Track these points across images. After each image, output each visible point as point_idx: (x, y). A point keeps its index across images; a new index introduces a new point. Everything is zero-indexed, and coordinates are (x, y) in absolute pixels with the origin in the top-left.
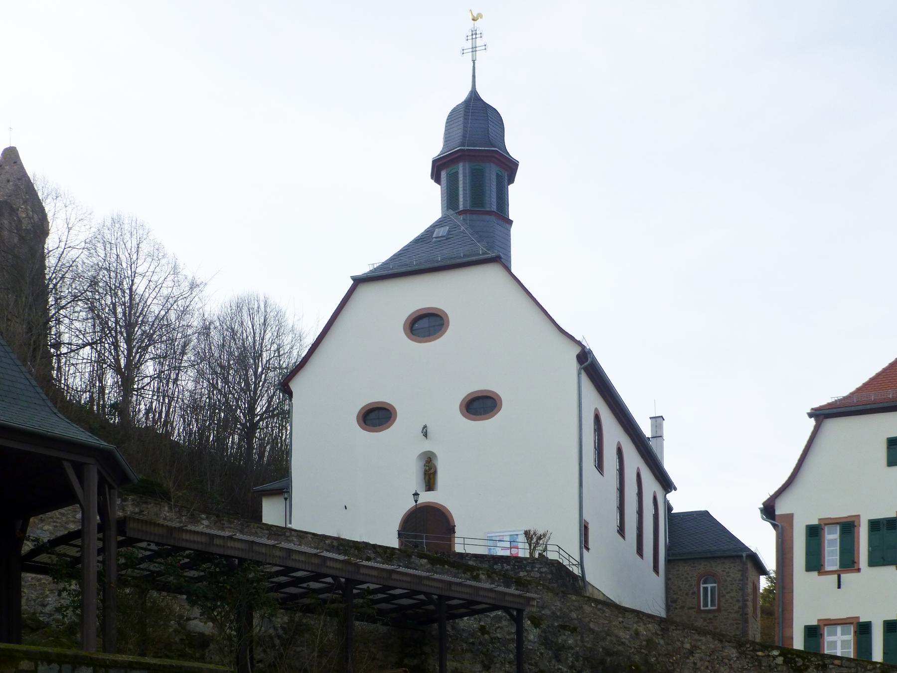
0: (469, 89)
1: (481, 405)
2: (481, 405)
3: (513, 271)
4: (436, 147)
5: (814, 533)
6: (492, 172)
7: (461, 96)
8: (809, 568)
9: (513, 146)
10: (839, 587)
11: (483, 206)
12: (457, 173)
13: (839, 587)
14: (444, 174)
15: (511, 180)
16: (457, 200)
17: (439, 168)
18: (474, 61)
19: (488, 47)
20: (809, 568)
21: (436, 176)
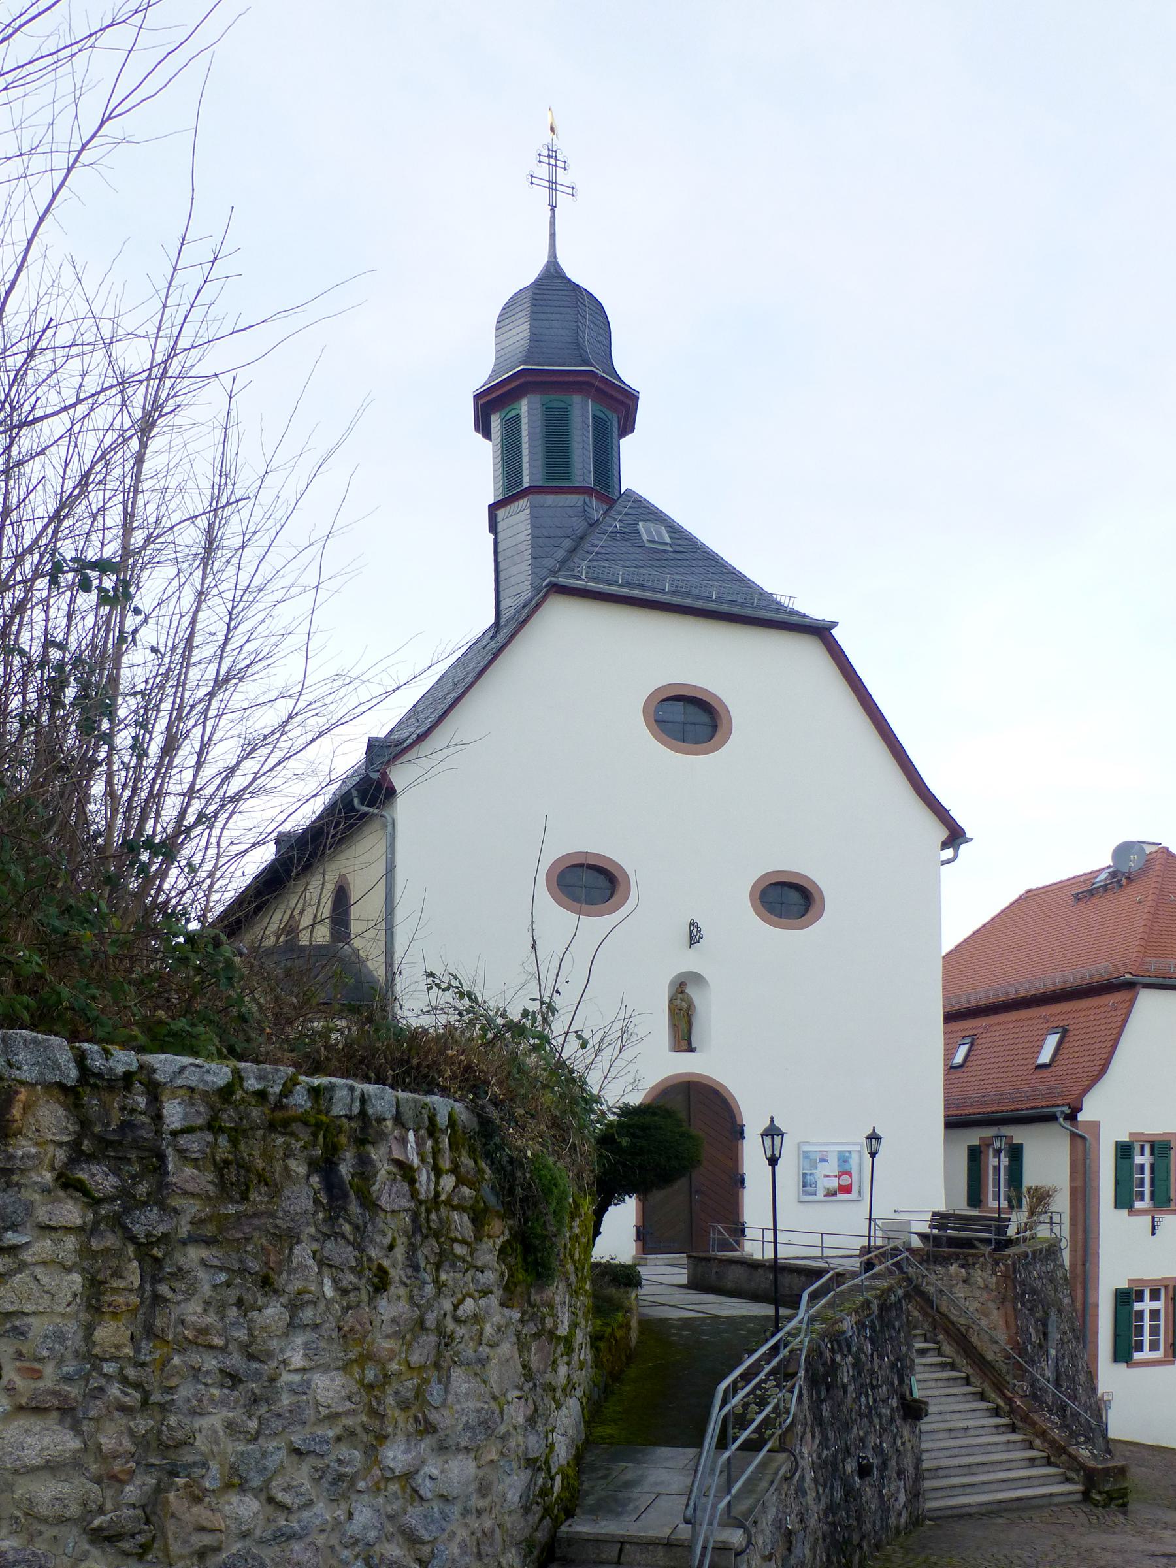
0: (544, 259)
1: (788, 899)
2: (788, 899)
3: (607, 1217)
4: (480, 369)
5: (1124, 1151)
6: (582, 412)
7: (530, 273)
8: (1118, 1205)
9: (629, 364)
10: (1153, 1234)
11: (567, 476)
12: (518, 417)
13: (1153, 1234)
14: (496, 422)
15: (627, 426)
16: (520, 454)
17: (491, 405)
18: (553, 208)
19: (579, 192)
20: (1118, 1205)
21: (483, 427)
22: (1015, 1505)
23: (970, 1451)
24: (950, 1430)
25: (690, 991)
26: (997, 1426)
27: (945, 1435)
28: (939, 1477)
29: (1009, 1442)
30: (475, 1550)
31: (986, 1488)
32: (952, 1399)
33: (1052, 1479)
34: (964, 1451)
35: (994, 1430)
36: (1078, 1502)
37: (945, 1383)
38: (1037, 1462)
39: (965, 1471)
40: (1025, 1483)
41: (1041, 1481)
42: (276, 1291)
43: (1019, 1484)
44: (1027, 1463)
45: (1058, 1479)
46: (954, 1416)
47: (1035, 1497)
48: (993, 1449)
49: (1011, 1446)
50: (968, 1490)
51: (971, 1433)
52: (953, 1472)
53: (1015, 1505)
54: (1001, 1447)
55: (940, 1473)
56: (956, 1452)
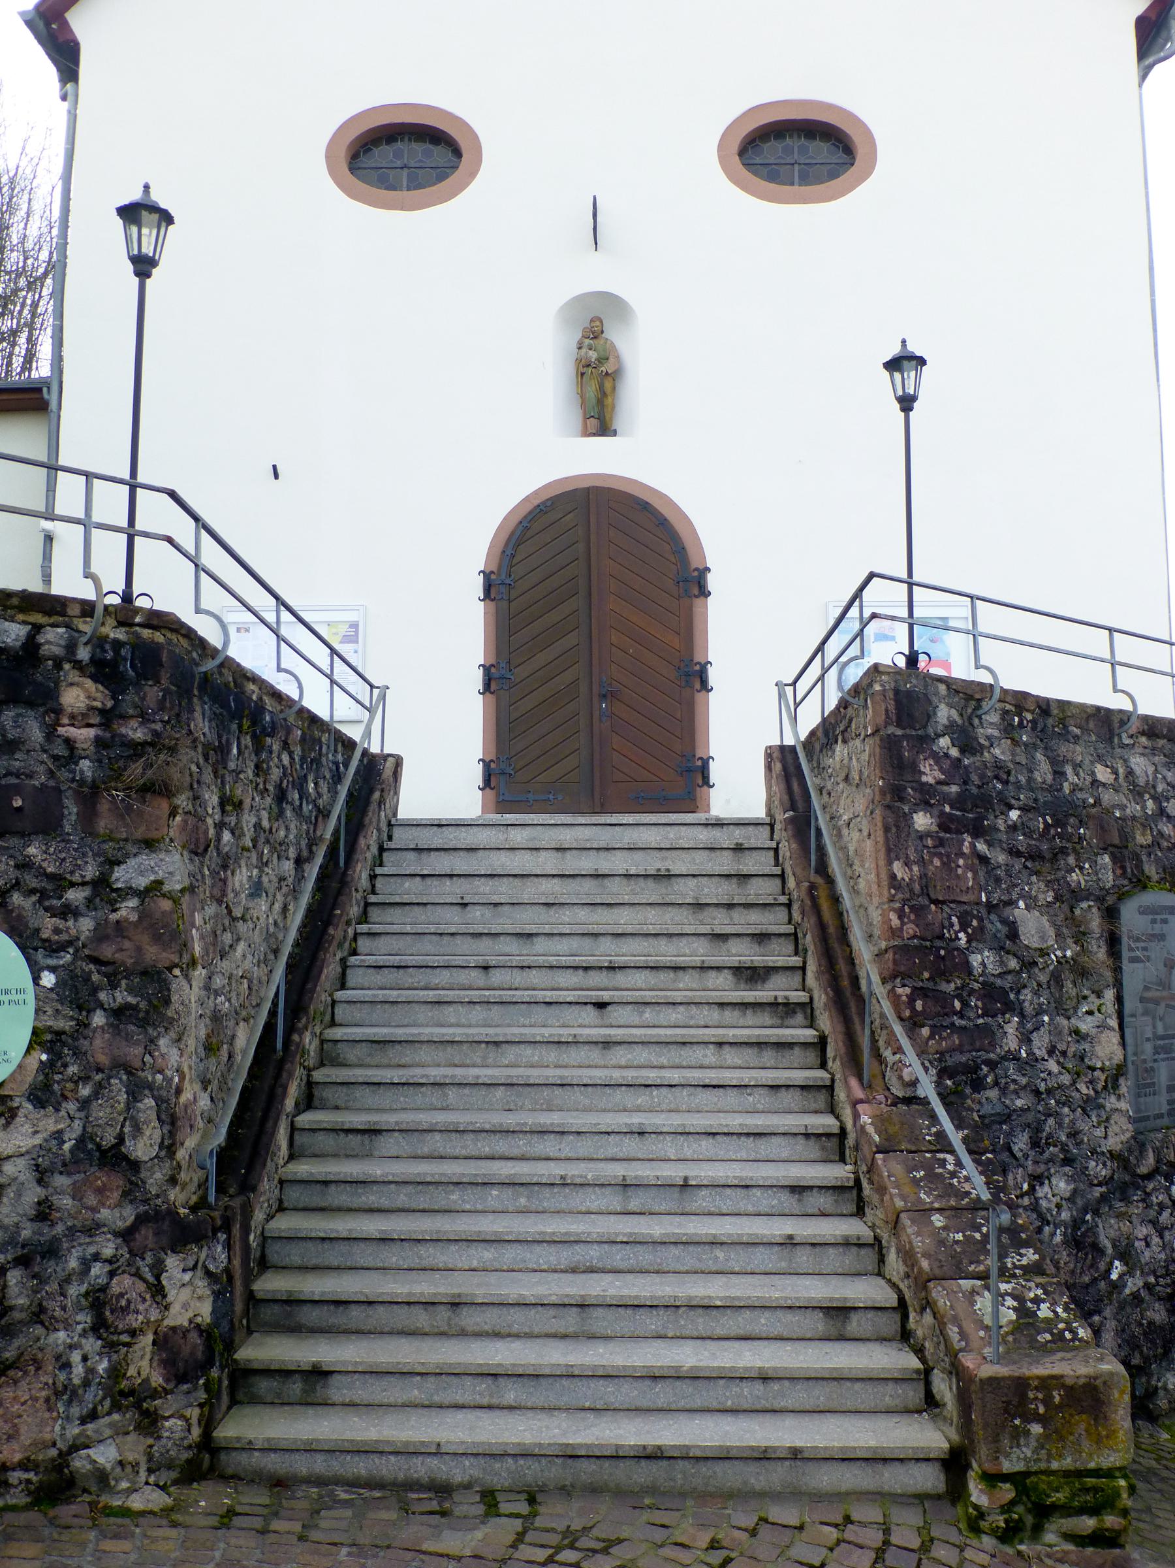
10: (274, 467)
13: (274, 467)
22: (644, 1474)
23: (645, 1257)
24: (625, 1185)
25: (616, 336)
26: (798, 1190)
27: (613, 1200)
28: (463, 1334)
29: (790, 1243)
30: (1035, 1469)
31: (589, 1393)
32: (731, 1098)
33: (865, 1396)
34: (619, 1257)
35: (787, 1201)
36: (921, 1498)
37: (749, 1055)
38: (855, 1324)
39: (570, 1321)
40: (749, 1393)
41: (820, 1395)
42: (158, 841)
43: (730, 1395)
44: (816, 1323)
45: (891, 1395)
46: (690, 1148)
47: (725, 1457)
48: (736, 1259)
49: (803, 1258)
50: (511, 1393)
51: (703, 1200)
52: (518, 1320)
53: (644, 1474)
54: (762, 1258)
55: (470, 1319)
56: (593, 1254)
